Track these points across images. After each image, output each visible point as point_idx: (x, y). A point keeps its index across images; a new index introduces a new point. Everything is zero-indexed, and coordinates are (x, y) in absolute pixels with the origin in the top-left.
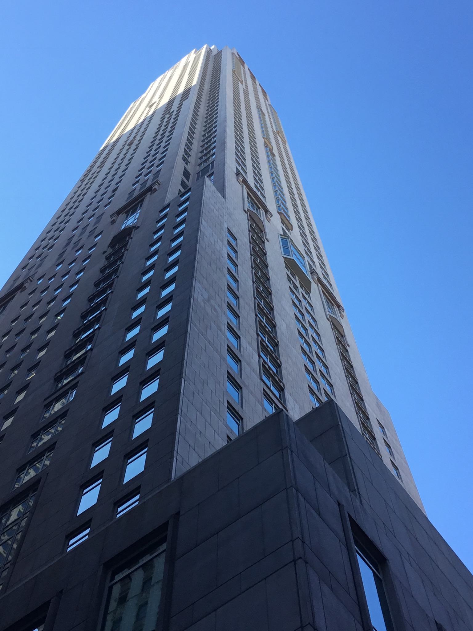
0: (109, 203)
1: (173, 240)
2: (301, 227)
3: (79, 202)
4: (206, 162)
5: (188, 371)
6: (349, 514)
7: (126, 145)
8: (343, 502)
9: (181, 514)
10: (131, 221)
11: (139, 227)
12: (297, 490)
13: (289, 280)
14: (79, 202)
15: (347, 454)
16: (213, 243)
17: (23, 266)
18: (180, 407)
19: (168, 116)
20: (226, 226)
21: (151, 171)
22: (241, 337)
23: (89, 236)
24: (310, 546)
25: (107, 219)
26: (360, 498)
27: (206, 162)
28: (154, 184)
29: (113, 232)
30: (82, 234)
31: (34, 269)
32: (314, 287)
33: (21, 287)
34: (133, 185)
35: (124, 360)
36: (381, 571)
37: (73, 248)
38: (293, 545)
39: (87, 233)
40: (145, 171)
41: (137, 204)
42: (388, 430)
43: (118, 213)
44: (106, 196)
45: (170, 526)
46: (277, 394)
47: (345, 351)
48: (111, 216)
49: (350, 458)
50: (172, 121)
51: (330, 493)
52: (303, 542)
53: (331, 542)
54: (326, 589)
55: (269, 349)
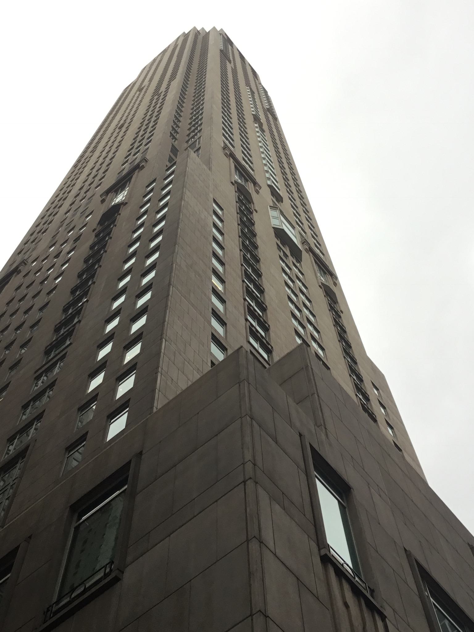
0: (99, 185)
1: (158, 212)
2: (292, 199)
3: (72, 186)
4: (194, 138)
5: (169, 332)
6: (310, 444)
7: (117, 129)
8: (305, 433)
9: (144, 452)
10: (120, 198)
11: (126, 203)
12: (252, 419)
13: (279, 248)
14: (72, 186)
15: (316, 392)
16: (198, 212)
17: (19, 252)
18: (160, 365)
19: (156, 97)
20: (211, 196)
21: (139, 150)
22: (227, 301)
23: (81, 217)
24: (262, 469)
25: (97, 199)
26: (326, 431)
27: (194, 138)
28: (141, 162)
29: (102, 209)
30: (74, 215)
31: (28, 253)
32: (305, 256)
33: (16, 271)
34: (123, 165)
35: (110, 327)
36: (344, 498)
37: (66, 229)
38: (244, 467)
39: (78, 214)
40: (133, 151)
41: (126, 183)
42: (383, 391)
43: (108, 192)
44: (97, 179)
45: (132, 465)
46: (265, 356)
47: (337, 317)
48: (101, 196)
49: (318, 396)
50: (160, 101)
51: (291, 424)
52: (255, 465)
53: (288, 469)
54: (277, 507)
55: (257, 314)
